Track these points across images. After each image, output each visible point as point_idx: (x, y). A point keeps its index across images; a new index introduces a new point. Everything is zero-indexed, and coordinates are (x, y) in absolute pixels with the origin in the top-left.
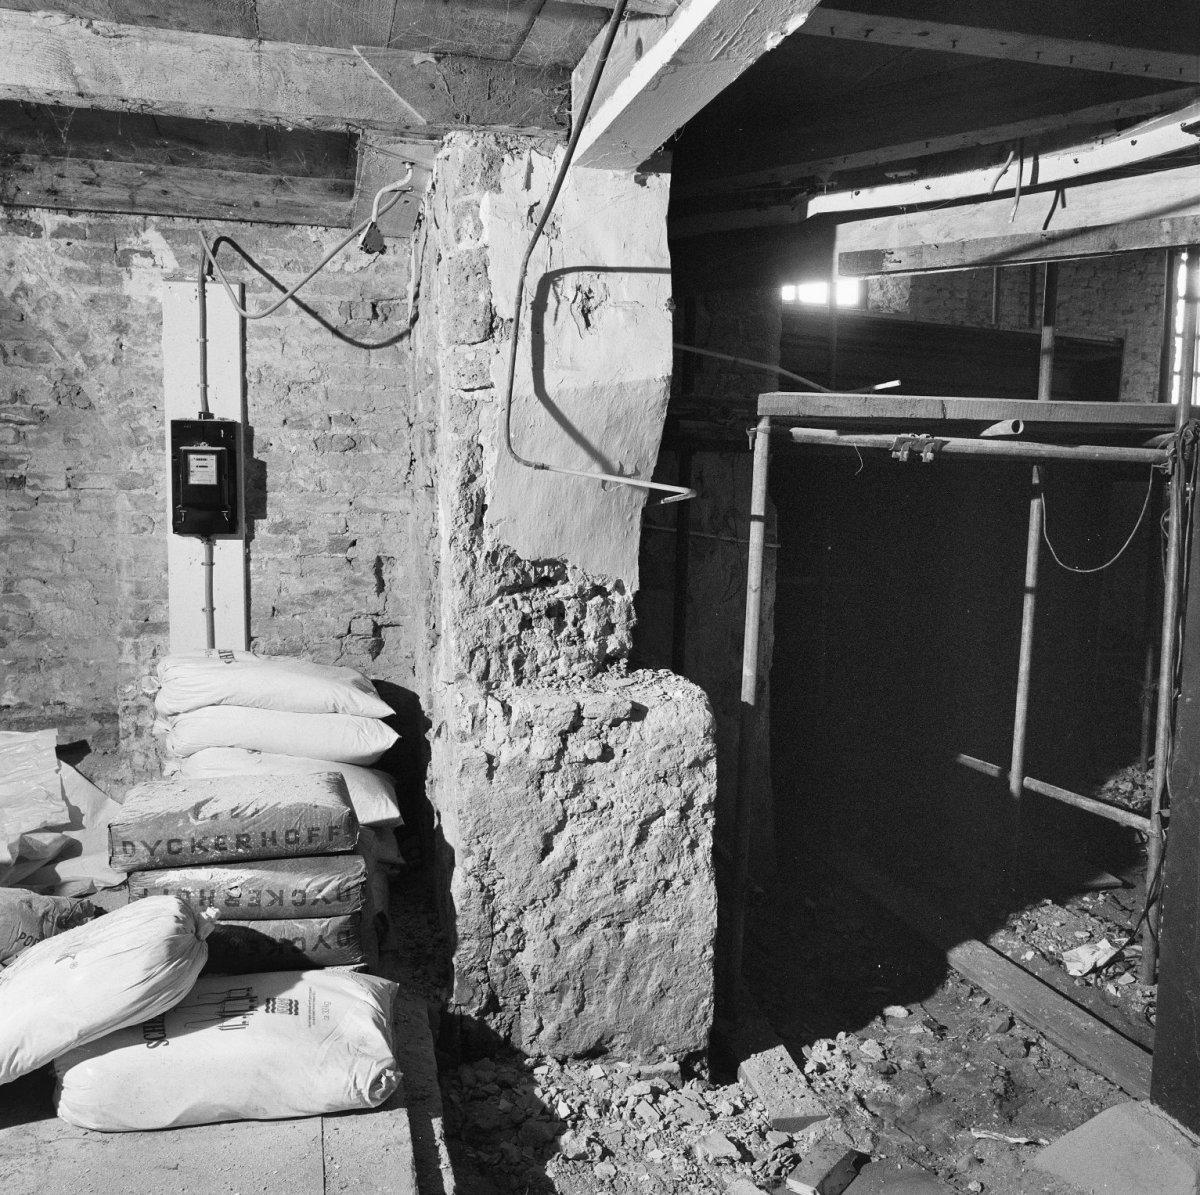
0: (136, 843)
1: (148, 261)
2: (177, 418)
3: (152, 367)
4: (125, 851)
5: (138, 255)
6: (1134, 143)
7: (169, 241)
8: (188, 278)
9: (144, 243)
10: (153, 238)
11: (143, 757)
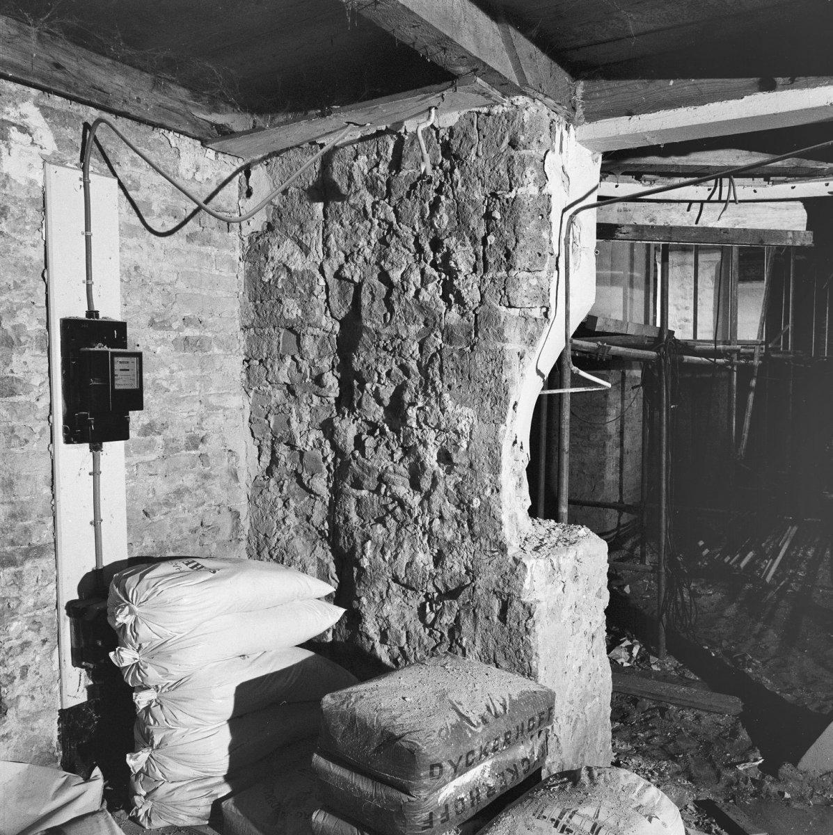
0: (444, 764)
1: (26, 138)
2: (67, 315)
3: (31, 258)
4: (432, 774)
5: (14, 128)
6: (793, 188)
7: (48, 120)
8: (68, 165)
9: (22, 116)
10: (34, 117)
11: (29, 700)
